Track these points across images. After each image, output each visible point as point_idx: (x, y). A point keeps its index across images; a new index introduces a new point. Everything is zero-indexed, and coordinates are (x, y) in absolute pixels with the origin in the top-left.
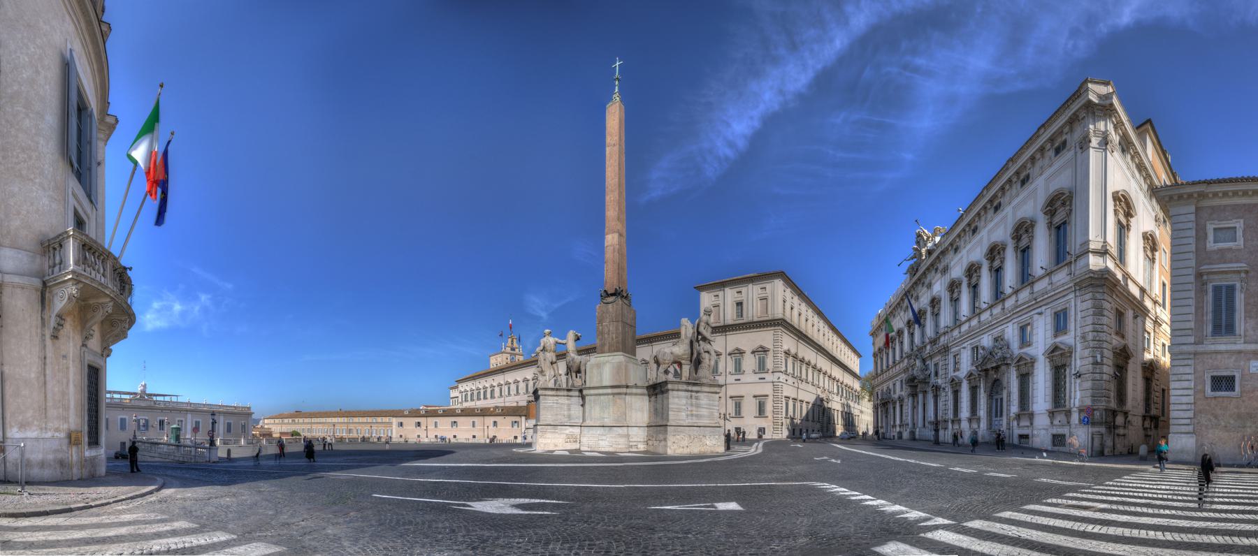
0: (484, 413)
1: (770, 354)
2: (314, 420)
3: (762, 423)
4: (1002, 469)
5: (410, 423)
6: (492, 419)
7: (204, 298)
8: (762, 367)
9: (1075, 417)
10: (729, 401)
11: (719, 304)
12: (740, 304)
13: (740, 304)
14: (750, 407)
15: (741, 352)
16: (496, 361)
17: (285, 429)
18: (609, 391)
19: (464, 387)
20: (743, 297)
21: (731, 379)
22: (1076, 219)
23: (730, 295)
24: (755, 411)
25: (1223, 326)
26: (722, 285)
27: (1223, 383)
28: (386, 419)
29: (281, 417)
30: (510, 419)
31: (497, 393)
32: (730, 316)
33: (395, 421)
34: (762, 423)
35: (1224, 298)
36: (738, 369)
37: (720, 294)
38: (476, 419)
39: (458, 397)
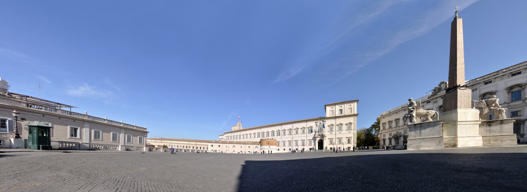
0: (245, 143)
1: (353, 125)
2: (172, 142)
3: (349, 145)
5: (216, 146)
8: (290, 134)
10: (337, 139)
11: (329, 111)
12: (341, 110)
13: (341, 110)
14: (300, 143)
15: (285, 130)
16: (237, 128)
18: (472, 123)
20: (343, 108)
21: (337, 133)
23: (338, 107)
24: (282, 145)
26: (335, 104)
30: (254, 146)
31: (238, 138)
32: (338, 114)
33: (210, 144)
34: (349, 145)
36: (297, 133)
37: (334, 107)
39: (224, 138)
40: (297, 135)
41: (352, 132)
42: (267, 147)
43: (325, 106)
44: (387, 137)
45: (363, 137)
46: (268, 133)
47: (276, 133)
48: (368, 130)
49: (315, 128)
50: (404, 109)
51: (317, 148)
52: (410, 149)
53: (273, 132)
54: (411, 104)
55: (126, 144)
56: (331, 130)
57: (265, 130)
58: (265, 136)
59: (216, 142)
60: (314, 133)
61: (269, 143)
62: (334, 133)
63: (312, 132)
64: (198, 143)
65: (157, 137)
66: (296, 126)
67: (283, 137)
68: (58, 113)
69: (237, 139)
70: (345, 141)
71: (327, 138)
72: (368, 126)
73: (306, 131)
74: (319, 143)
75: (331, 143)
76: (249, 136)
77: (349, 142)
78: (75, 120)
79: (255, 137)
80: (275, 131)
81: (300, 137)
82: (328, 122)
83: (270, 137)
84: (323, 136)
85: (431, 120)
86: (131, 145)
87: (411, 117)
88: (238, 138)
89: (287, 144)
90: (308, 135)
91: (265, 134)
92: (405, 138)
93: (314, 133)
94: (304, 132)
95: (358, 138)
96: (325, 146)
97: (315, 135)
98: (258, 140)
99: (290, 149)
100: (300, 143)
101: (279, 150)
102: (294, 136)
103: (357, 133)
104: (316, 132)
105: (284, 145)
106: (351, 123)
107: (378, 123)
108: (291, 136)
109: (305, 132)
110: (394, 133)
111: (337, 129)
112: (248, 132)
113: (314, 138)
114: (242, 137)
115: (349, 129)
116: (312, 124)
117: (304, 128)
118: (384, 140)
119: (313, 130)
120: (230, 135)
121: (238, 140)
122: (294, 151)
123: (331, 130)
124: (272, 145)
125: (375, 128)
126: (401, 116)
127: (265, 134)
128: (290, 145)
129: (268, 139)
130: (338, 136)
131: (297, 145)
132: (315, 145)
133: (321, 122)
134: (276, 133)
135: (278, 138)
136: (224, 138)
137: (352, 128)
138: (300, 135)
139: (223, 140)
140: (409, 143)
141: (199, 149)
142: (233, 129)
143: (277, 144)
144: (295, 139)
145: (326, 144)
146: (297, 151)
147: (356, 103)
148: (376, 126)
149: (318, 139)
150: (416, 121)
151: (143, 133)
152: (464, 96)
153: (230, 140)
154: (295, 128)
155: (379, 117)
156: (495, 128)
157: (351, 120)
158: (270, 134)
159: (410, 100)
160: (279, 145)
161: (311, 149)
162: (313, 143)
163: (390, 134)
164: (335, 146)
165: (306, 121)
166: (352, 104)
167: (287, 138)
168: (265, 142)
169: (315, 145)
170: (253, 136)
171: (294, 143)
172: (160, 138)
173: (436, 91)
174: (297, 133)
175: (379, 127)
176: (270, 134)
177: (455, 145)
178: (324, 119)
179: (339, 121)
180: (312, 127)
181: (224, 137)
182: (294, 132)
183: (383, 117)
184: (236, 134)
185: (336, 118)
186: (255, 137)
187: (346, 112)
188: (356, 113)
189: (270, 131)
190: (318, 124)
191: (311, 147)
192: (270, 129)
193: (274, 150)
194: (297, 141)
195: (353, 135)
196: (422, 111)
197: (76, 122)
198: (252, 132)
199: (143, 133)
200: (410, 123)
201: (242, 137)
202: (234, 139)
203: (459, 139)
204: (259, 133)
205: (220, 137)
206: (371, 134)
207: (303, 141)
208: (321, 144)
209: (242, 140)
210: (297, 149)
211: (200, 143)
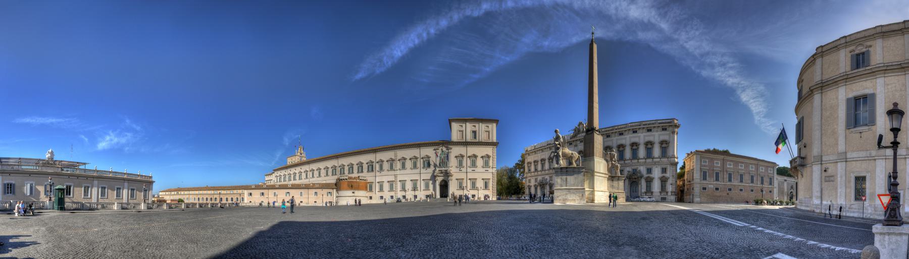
3: (486, 192)
4: (609, 159)
5: (256, 193)
6: (314, 191)
7: (129, 135)
8: (392, 168)
9: (669, 194)
11: (456, 131)
12: (474, 132)
13: (474, 132)
14: (409, 186)
16: (296, 159)
17: (172, 198)
19: (276, 174)
20: (477, 129)
21: (469, 170)
22: (670, 149)
23: (469, 127)
24: (378, 189)
25: (705, 179)
26: (465, 121)
27: (704, 189)
28: (240, 191)
29: (170, 191)
30: (325, 191)
31: (297, 178)
32: (469, 138)
33: (246, 192)
34: (486, 192)
35: (705, 173)
36: (403, 167)
38: (302, 191)
39: (273, 179)
40: (403, 172)
41: (490, 170)
42: (349, 193)
43: (450, 121)
44: (533, 183)
45: (505, 180)
46: (351, 166)
47: (365, 167)
48: (511, 170)
49: (434, 159)
50: (548, 146)
51: (438, 196)
52: (558, 204)
53: (360, 165)
54: (557, 138)
55: (100, 201)
56: (460, 164)
57: (345, 161)
58: (346, 172)
59: (258, 187)
60: (432, 168)
61: (353, 186)
62: (464, 170)
63: (429, 165)
64: (223, 192)
65: (173, 188)
66: (401, 153)
67: (378, 174)
68: (78, 172)
69: (295, 179)
70: (480, 184)
71: (454, 178)
72: (511, 165)
73: (420, 163)
74: (441, 186)
75: (461, 187)
76: (316, 173)
77: (486, 187)
78: (87, 177)
79: (327, 174)
80: (365, 162)
81: (408, 175)
82: (456, 151)
83: (355, 175)
84: (447, 174)
85: (575, 165)
86: (107, 201)
87: (557, 157)
88: (297, 178)
89: (386, 187)
90: (423, 171)
91: (346, 168)
92: (551, 186)
93: (432, 168)
94: (415, 166)
95: (499, 182)
96: (450, 192)
97: (434, 171)
98: (332, 180)
99: (392, 197)
100: (409, 186)
101: (371, 198)
102: (398, 172)
103: (498, 174)
104: (435, 166)
105: (381, 189)
106: (488, 156)
107: (523, 162)
108: (392, 172)
109: (418, 165)
110: (539, 178)
111: (469, 164)
112: (314, 166)
113: (434, 178)
114: (304, 175)
115: (486, 165)
116: (429, 152)
117: (416, 158)
118: (530, 187)
119: (432, 163)
120: (283, 173)
121: (298, 182)
122: (399, 201)
123: (460, 164)
124: (358, 188)
125: (520, 168)
126: (546, 155)
127: (346, 168)
128: (391, 189)
129: (350, 178)
130: (470, 176)
131: (404, 189)
132: (434, 189)
133: (444, 149)
134: (365, 167)
135: (368, 177)
136: (273, 179)
137: (491, 164)
138: (408, 171)
139: (272, 183)
140: (556, 194)
141: (224, 201)
142: (290, 161)
143: (368, 187)
144: (400, 178)
145: (453, 189)
146: (403, 200)
147: (495, 125)
148: (520, 165)
149: (439, 179)
150: (563, 163)
151: (147, 184)
152: (598, 140)
153: (283, 183)
154: (399, 157)
155: (524, 152)
156: (615, 183)
157: (489, 150)
158: (355, 167)
159: (556, 131)
160: (371, 190)
161: (427, 196)
162: (431, 186)
163: (536, 180)
164: (466, 192)
165: (419, 146)
166: (490, 126)
167: (385, 177)
168: (345, 184)
169: (434, 189)
170: (323, 172)
171: (399, 185)
172: (176, 187)
173: (577, 131)
174: (403, 167)
175: (524, 168)
176: (355, 167)
177: (593, 201)
178: (448, 143)
179: (472, 150)
180: (428, 157)
181: (273, 177)
182: (398, 165)
183: (528, 153)
184: (292, 171)
185: (466, 144)
186: (327, 174)
187: (483, 137)
188: (495, 140)
189: (355, 163)
190: (439, 151)
191: (429, 193)
192: (354, 160)
193: (363, 196)
194: (403, 183)
195: (490, 174)
196: (567, 151)
197: (89, 179)
198: (322, 165)
199: (147, 184)
200: (556, 166)
201: (304, 175)
202: (290, 180)
203: (596, 193)
204: (334, 168)
205: (267, 178)
206: (515, 177)
207: (414, 182)
208: (444, 187)
209: (304, 181)
210: (404, 197)
211: (225, 192)
